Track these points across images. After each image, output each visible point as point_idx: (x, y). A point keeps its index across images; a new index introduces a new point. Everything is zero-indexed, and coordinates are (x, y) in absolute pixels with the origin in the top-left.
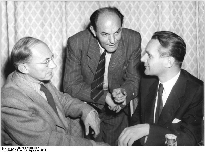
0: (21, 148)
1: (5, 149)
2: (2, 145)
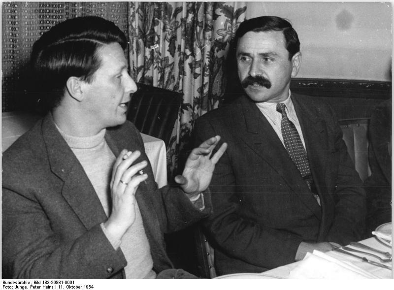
0: (40, 283)
1: (10, 285)
2: (3, 278)
